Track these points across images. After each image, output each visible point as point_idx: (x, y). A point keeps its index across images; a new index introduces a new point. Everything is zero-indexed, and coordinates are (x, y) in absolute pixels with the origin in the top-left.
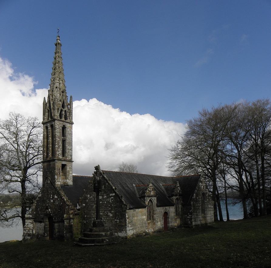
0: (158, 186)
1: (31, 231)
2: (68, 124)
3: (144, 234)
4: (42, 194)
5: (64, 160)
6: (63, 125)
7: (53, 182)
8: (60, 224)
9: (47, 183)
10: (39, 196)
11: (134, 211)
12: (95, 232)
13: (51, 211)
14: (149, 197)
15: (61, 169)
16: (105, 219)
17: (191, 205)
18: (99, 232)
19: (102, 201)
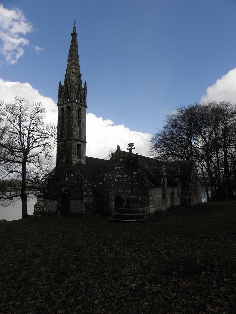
1: (42, 208)
6: (79, 108)
7: (69, 160)
8: (77, 201)
10: (52, 174)
12: (133, 208)
13: (66, 189)
15: (76, 149)
16: (125, 196)
17: (190, 186)
19: (122, 180)
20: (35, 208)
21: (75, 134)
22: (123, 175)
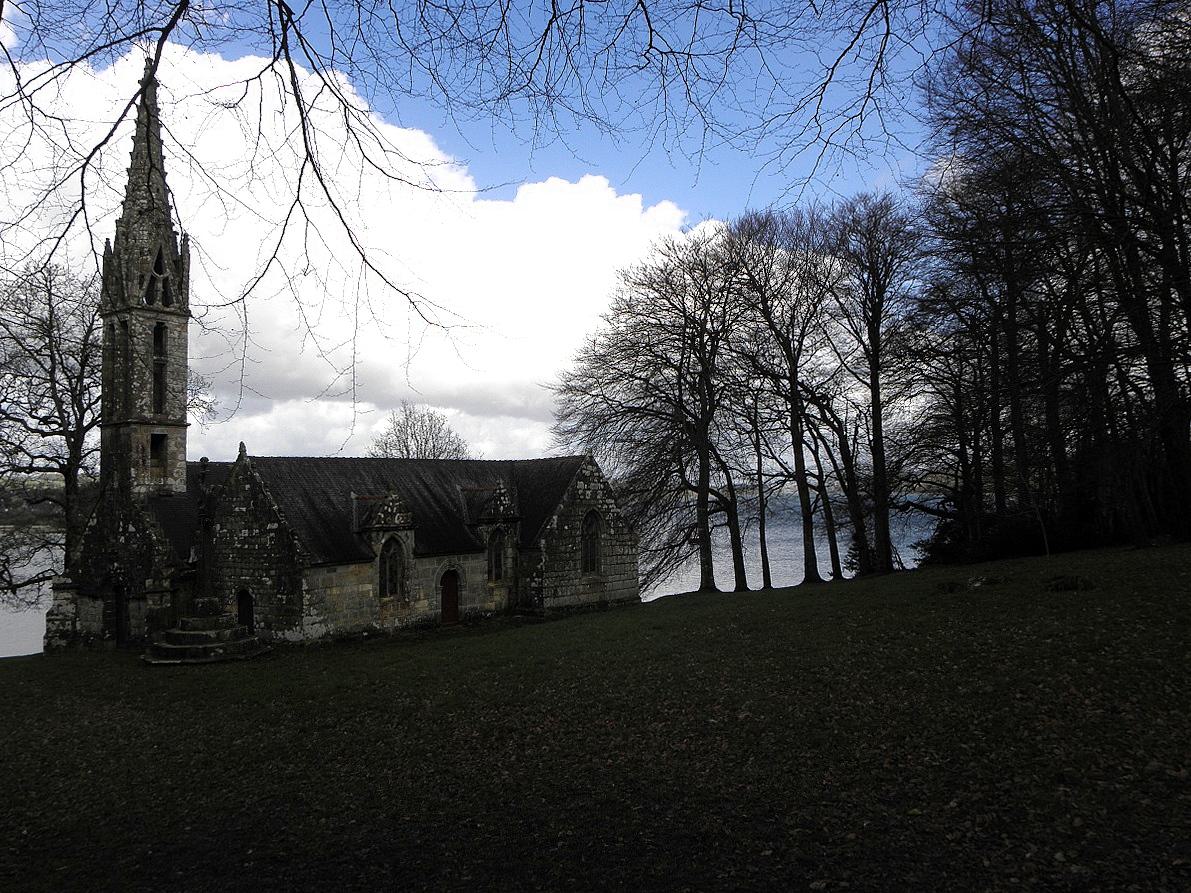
0: (446, 492)
1: (70, 622)
2: (174, 318)
3: (365, 634)
4: (97, 517)
5: (160, 424)
7: (125, 486)
9: (112, 489)
11: (328, 572)
14: (386, 530)
18: (203, 630)
20: (48, 621)
21: (141, 406)
22: (251, 529)
